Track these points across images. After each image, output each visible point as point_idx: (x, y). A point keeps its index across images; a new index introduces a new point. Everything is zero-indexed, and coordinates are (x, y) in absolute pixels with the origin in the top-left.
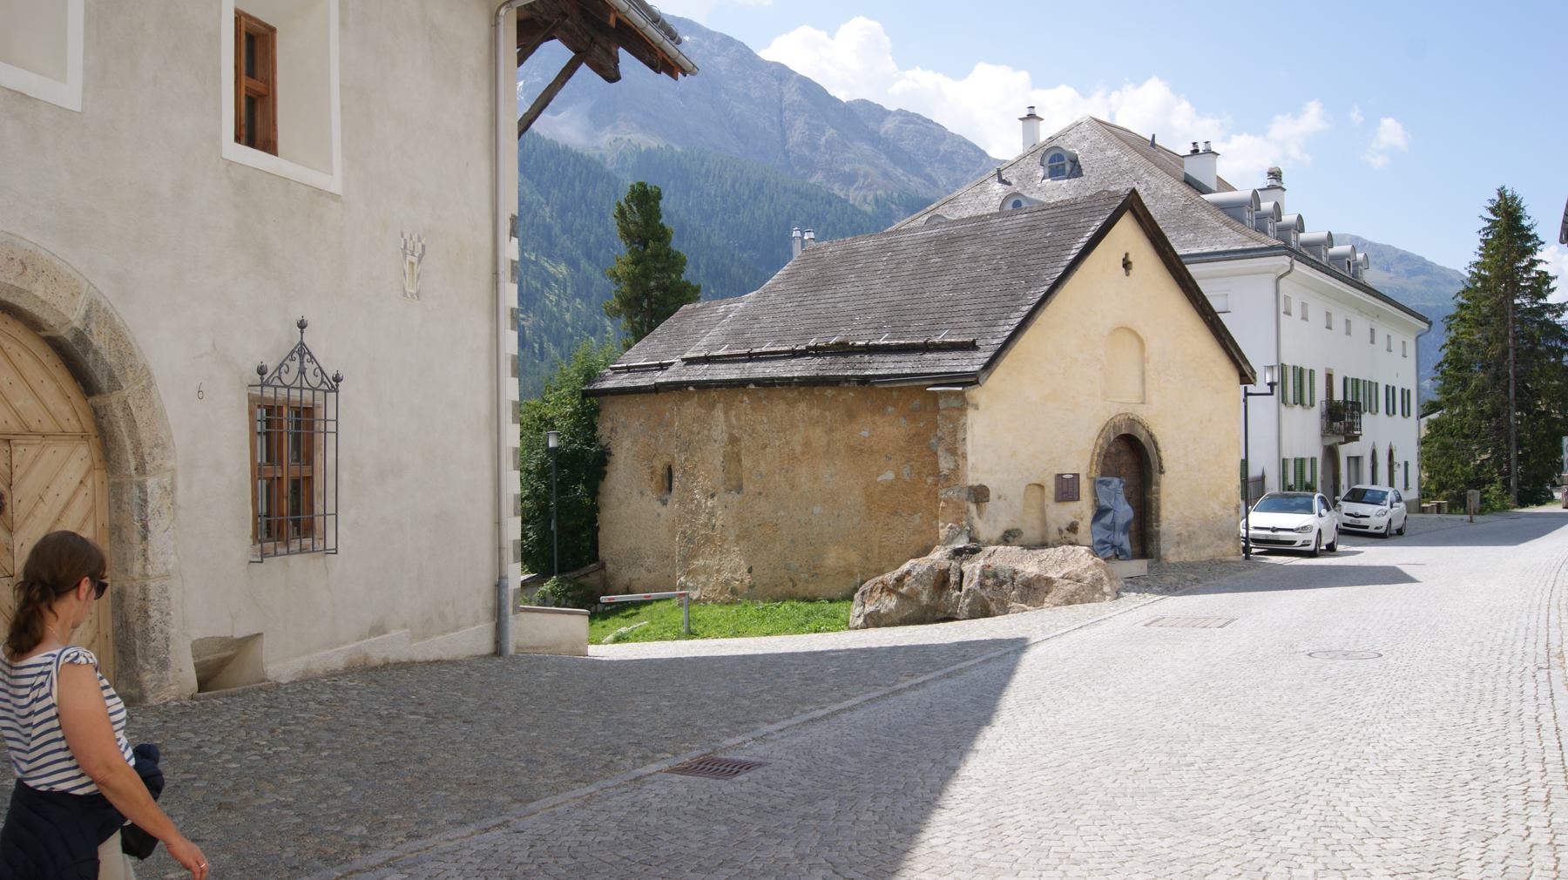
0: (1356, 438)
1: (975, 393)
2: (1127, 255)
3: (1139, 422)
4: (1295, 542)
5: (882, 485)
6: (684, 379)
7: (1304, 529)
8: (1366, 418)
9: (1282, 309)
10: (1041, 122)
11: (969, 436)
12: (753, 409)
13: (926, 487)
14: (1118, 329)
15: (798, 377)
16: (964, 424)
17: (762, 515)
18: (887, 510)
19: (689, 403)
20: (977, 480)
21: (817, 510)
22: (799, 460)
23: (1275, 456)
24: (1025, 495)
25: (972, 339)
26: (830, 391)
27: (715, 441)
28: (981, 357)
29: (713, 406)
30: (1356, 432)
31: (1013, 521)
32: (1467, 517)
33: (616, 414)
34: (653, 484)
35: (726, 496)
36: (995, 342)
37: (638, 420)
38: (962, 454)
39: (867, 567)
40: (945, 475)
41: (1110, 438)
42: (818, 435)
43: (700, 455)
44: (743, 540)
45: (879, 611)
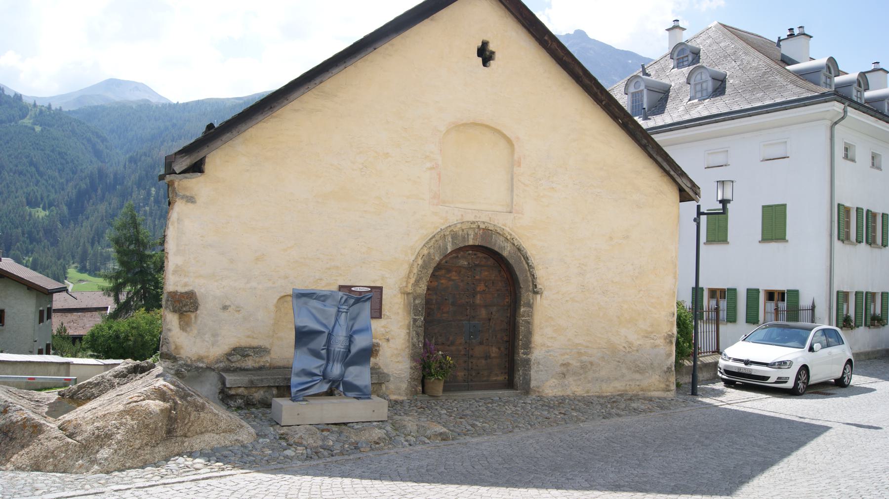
4: (768, 378)
7: (781, 364)
23: (826, 288)
31: (248, 337)
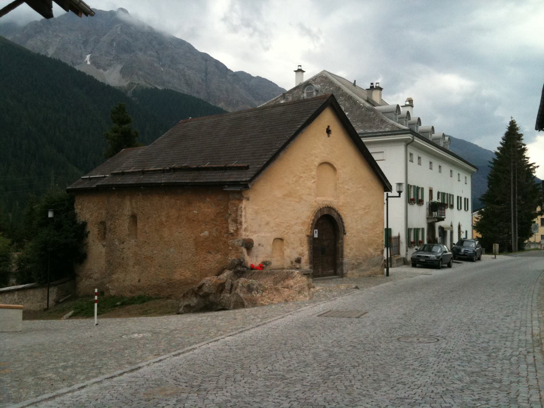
0: (443, 219)
2: (329, 127)
5: (203, 238)
6: (111, 183)
8: (448, 211)
9: (409, 159)
10: (304, 73)
15: (164, 183)
22: (164, 225)
25: (247, 165)
28: (250, 173)
30: (442, 217)
32: (493, 256)
36: (258, 166)
38: (240, 223)
41: (318, 216)
45: (190, 305)
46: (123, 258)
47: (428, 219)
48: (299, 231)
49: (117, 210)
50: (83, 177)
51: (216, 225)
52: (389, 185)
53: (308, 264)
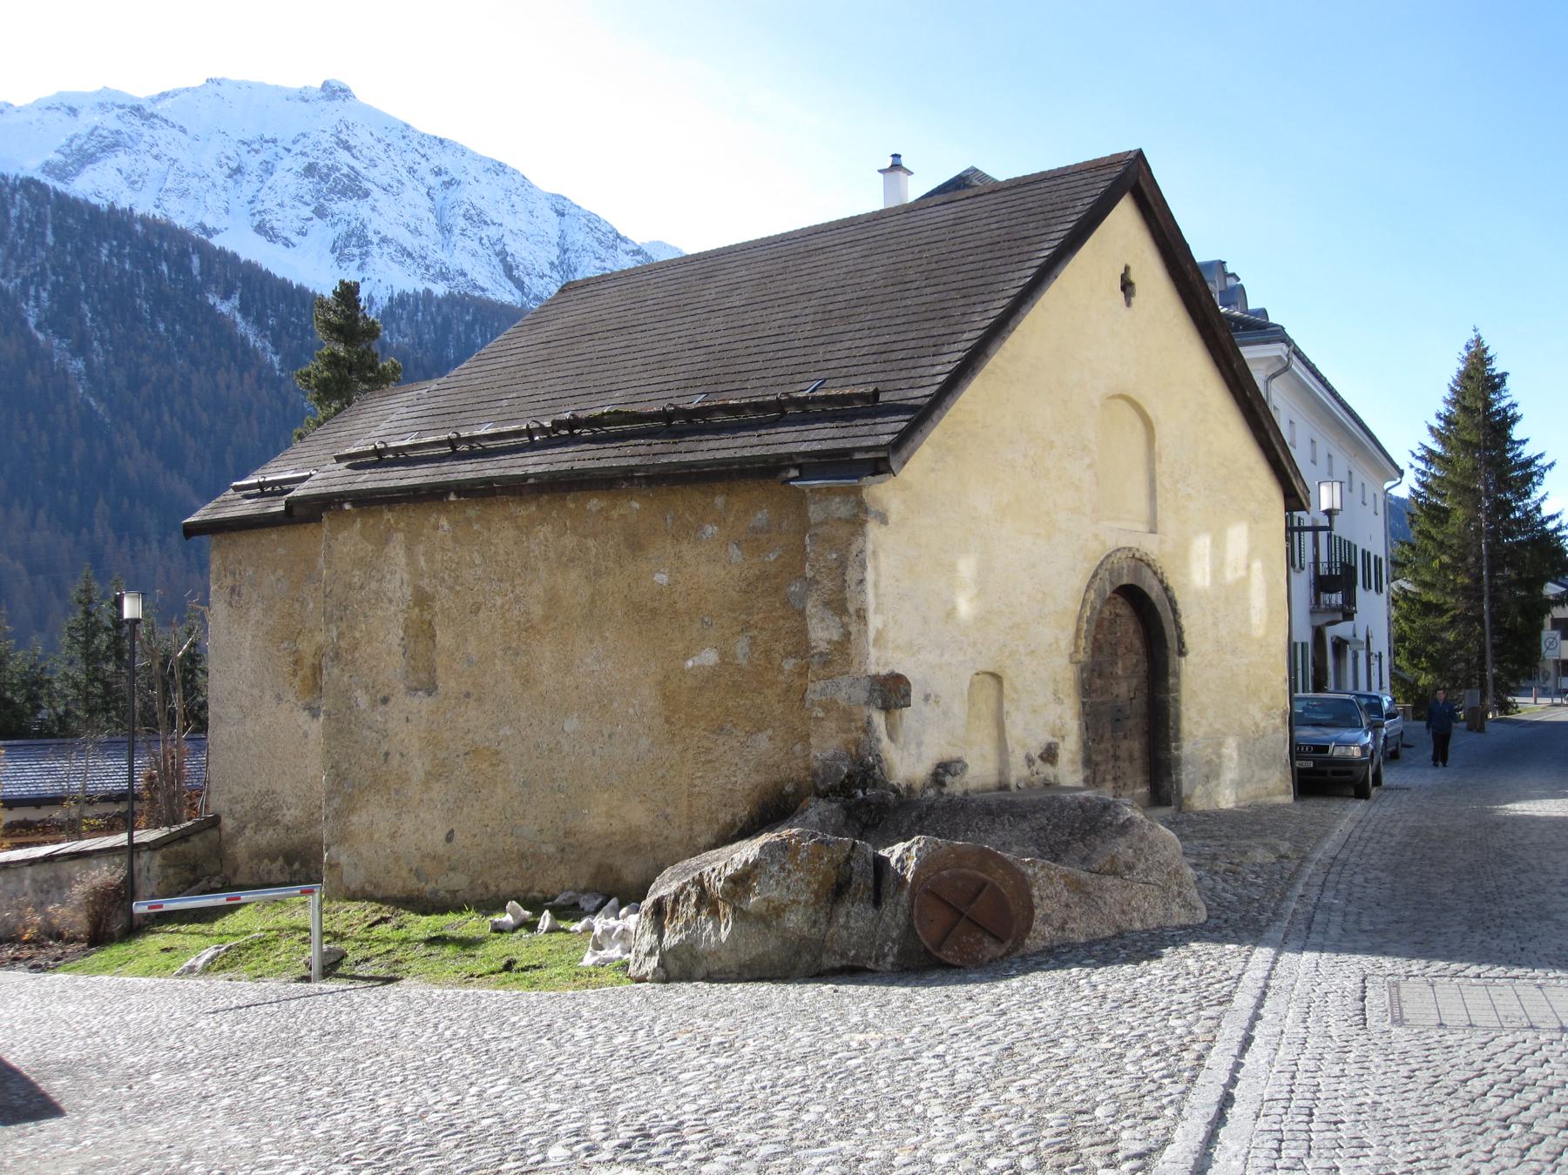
1: (880, 491)
2: (1127, 268)
3: (1149, 565)
11: (870, 576)
12: (456, 540)
13: (781, 678)
14: (1113, 397)
15: (535, 475)
16: (861, 551)
17: (470, 736)
18: (702, 724)
19: (346, 534)
20: (886, 664)
21: (571, 725)
24: (970, 694)
25: (871, 389)
26: (595, 501)
27: (391, 601)
29: (385, 540)
33: (240, 563)
34: (297, 682)
35: (407, 700)
37: (274, 572)
39: (666, 833)
40: (821, 654)
42: (572, 583)
43: (363, 626)
44: (438, 780)
46: (387, 754)
47: (1312, 612)
48: (1050, 645)
49: (359, 584)
50: (238, 483)
51: (747, 626)
52: (1301, 484)
53: (1080, 767)
